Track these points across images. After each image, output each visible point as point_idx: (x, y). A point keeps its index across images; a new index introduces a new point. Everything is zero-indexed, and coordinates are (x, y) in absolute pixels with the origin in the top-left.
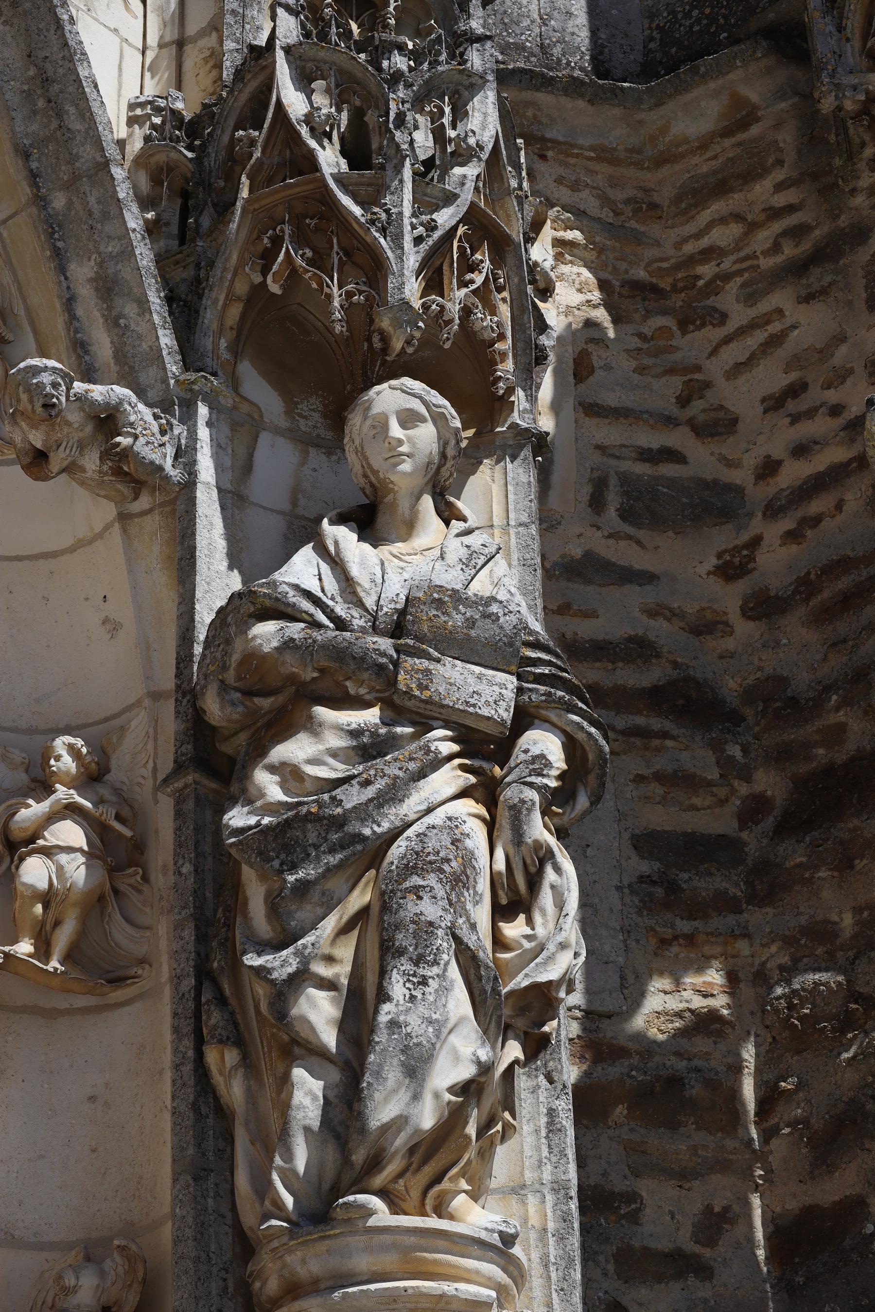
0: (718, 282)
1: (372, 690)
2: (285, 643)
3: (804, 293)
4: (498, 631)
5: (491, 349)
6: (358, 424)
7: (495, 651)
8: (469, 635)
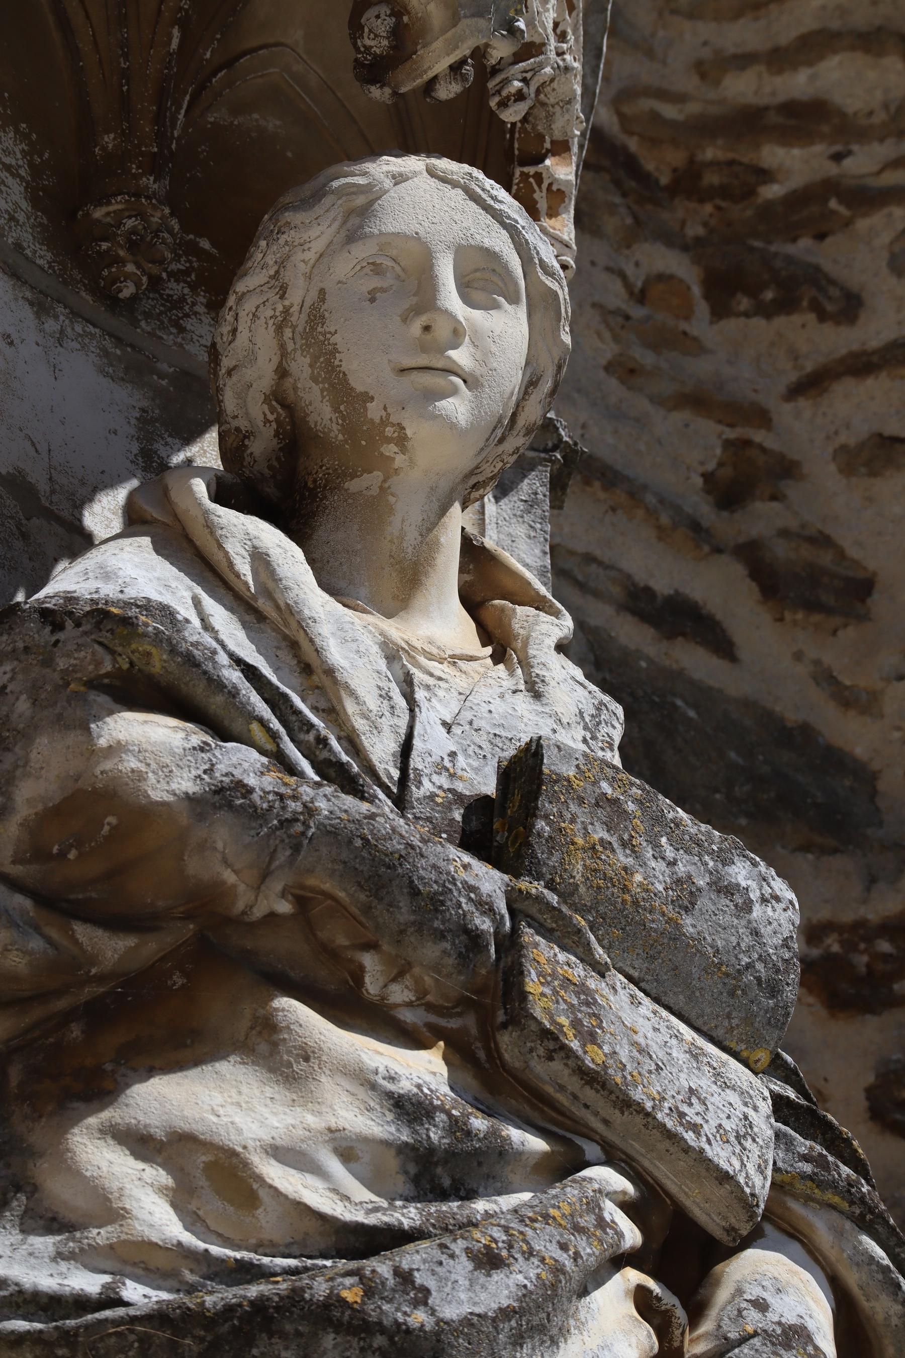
0: (833, 204)
1: (421, 1001)
2: (219, 791)
4: (747, 940)
5: (531, 170)
6: (318, 246)
7: (732, 994)
8: (678, 926)
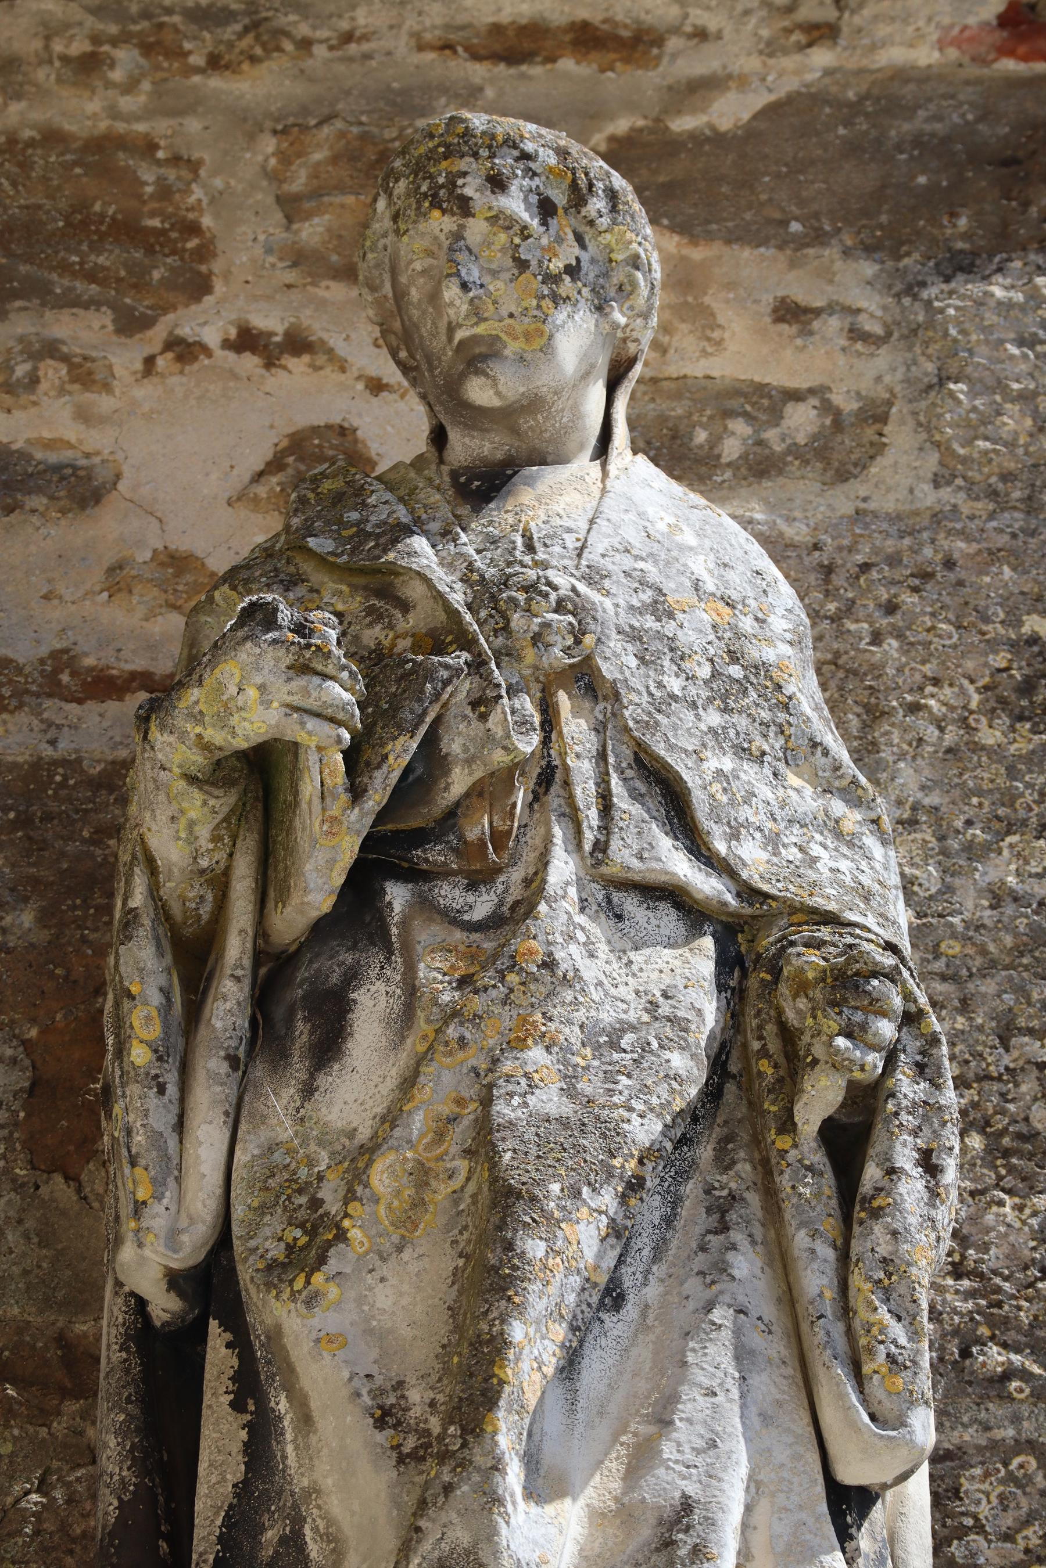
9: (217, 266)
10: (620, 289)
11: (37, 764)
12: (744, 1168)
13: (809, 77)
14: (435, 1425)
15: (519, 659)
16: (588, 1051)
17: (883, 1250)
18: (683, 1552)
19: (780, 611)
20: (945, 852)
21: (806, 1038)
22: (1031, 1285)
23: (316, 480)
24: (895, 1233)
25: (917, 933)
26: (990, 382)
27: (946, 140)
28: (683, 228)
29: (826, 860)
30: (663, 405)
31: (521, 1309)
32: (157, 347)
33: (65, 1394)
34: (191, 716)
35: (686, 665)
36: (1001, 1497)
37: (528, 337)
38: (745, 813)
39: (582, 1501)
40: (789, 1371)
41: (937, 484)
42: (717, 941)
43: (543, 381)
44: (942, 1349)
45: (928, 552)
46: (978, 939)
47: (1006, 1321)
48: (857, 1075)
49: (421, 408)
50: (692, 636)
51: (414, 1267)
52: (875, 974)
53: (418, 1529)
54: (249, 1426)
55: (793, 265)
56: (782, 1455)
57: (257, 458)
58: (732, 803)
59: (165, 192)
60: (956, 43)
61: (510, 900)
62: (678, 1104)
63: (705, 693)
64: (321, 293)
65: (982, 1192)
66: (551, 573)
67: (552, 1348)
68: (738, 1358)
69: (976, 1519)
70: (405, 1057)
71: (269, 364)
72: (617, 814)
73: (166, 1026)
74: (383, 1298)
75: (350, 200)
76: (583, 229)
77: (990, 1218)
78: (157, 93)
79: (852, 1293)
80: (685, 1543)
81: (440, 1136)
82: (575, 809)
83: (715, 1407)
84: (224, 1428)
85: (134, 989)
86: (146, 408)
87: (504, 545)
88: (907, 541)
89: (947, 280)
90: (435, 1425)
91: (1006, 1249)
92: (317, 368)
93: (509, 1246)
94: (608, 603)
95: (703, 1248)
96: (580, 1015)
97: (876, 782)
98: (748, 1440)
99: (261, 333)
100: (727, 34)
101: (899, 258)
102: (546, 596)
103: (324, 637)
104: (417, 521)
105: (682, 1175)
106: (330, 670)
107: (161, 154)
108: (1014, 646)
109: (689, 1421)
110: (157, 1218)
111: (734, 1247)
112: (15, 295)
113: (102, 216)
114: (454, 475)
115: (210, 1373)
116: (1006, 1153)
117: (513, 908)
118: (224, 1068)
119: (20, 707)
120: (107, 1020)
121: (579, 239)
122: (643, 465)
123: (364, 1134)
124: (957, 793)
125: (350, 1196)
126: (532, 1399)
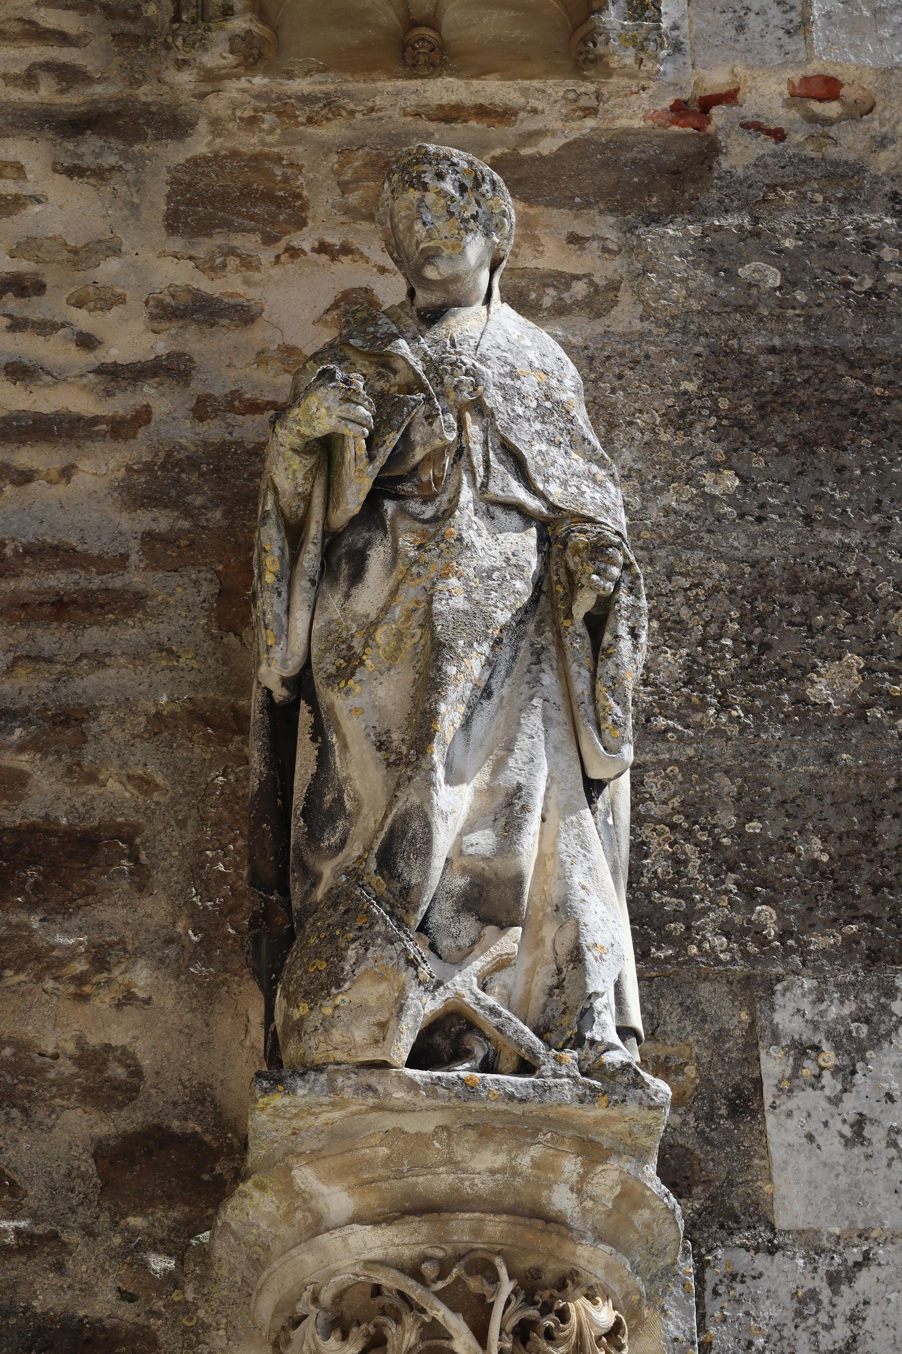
3: (68, 162)
9: (310, 214)
10: (497, 226)
11: (224, 443)
12: (549, 635)
13: (584, 132)
14: (404, 750)
15: (448, 397)
16: (477, 580)
17: (612, 673)
18: (517, 808)
19: (569, 377)
20: (643, 490)
21: (578, 575)
22: (679, 690)
23: (354, 312)
24: (617, 665)
25: (630, 528)
26: (667, 273)
27: (647, 162)
28: (525, 199)
29: (589, 493)
30: (516, 281)
31: (445, 698)
32: (281, 251)
33: (235, 732)
34: (295, 421)
35: (525, 401)
36: (662, 785)
37: (453, 247)
38: (552, 470)
39: (471, 785)
40: (568, 727)
41: (642, 320)
42: (538, 530)
43: (461, 268)
44: (637, 718)
45: (637, 351)
46: (658, 531)
47: (667, 706)
48: (602, 592)
49: (404, 281)
50: (528, 388)
51: (395, 678)
52: (611, 546)
53: (396, 796)
54: (319, 749)
55: (576, 217)
56: (563, 765)
57: (327, 303)
58: (546, 466)
59: (286, 179)
60: (651, 118)
61: (442, 509)
62: (519, 605)
63: (534, 415)
64: (358, 227)
65: (657, 647)
66: (463, 357)
67: (458, 716)
68: (544, 721)
69: (651, 794)
70: (392, 582)
71: (333, 259)
72: (492, 470)
73: (282, 565)
74: (381, 692)
75: (372, 184)
76: (479, 198)
77: (660, 659)
78: (283, 134)
79: (597, 692)
80: (518, 804)
81: (408, 618)
82: (473, 467)
83: (533, 743)
84: (307, 749)
85: (267, 548)
86: (276, 279)
87: (441, 344)
88: (628, 346)
89: (647, 226)
90: (404, 750)
91: (667, 673)
92: (355, 261)
93: (440, 669)
94: (489, 372)
95: (529, 671)
96: (474, 563)
97: (612, 458)
98: (548, 759)
99: (330, 245)
100: (547, 111)
101: (625, 215)
102: (460, 368)
103: (357, 385)
104: (401, 332)
105: (520, 638)
106: (360, 401)
107: (284, 162)
108: (676, 395)
109: (521, 749)
110: (277, 653)
111: (543, 671)
112: (217, 226)
113: (257, 190)
114: (418, 311)
115: (301, 724)
116: (669, 630)
117: (443, 513)
118: (308, 585)
119: (216, 416)
120: (255, 562)
121: (478, 203)
122: (506, 308)
123: (373, 616)
124: (649, 463)
125: (366, 645)
126: (449, 739)
